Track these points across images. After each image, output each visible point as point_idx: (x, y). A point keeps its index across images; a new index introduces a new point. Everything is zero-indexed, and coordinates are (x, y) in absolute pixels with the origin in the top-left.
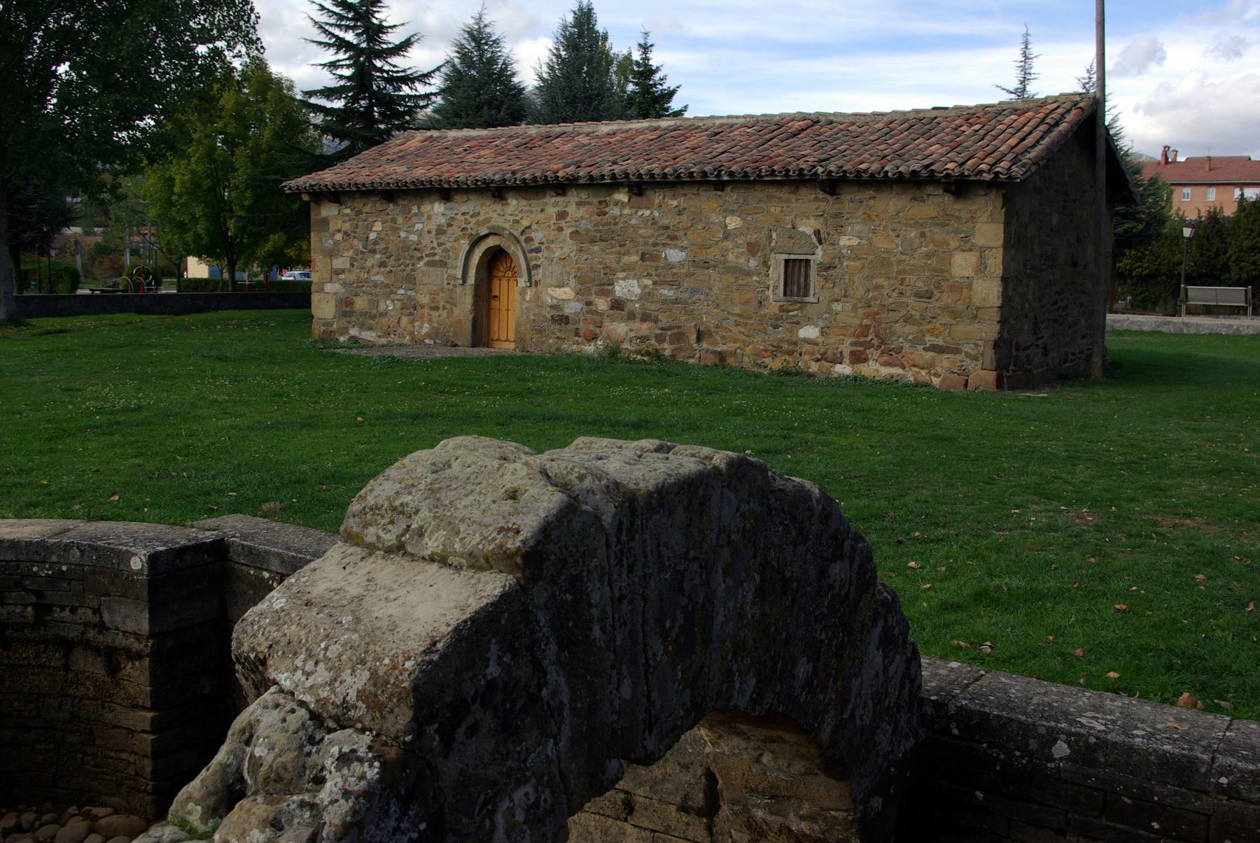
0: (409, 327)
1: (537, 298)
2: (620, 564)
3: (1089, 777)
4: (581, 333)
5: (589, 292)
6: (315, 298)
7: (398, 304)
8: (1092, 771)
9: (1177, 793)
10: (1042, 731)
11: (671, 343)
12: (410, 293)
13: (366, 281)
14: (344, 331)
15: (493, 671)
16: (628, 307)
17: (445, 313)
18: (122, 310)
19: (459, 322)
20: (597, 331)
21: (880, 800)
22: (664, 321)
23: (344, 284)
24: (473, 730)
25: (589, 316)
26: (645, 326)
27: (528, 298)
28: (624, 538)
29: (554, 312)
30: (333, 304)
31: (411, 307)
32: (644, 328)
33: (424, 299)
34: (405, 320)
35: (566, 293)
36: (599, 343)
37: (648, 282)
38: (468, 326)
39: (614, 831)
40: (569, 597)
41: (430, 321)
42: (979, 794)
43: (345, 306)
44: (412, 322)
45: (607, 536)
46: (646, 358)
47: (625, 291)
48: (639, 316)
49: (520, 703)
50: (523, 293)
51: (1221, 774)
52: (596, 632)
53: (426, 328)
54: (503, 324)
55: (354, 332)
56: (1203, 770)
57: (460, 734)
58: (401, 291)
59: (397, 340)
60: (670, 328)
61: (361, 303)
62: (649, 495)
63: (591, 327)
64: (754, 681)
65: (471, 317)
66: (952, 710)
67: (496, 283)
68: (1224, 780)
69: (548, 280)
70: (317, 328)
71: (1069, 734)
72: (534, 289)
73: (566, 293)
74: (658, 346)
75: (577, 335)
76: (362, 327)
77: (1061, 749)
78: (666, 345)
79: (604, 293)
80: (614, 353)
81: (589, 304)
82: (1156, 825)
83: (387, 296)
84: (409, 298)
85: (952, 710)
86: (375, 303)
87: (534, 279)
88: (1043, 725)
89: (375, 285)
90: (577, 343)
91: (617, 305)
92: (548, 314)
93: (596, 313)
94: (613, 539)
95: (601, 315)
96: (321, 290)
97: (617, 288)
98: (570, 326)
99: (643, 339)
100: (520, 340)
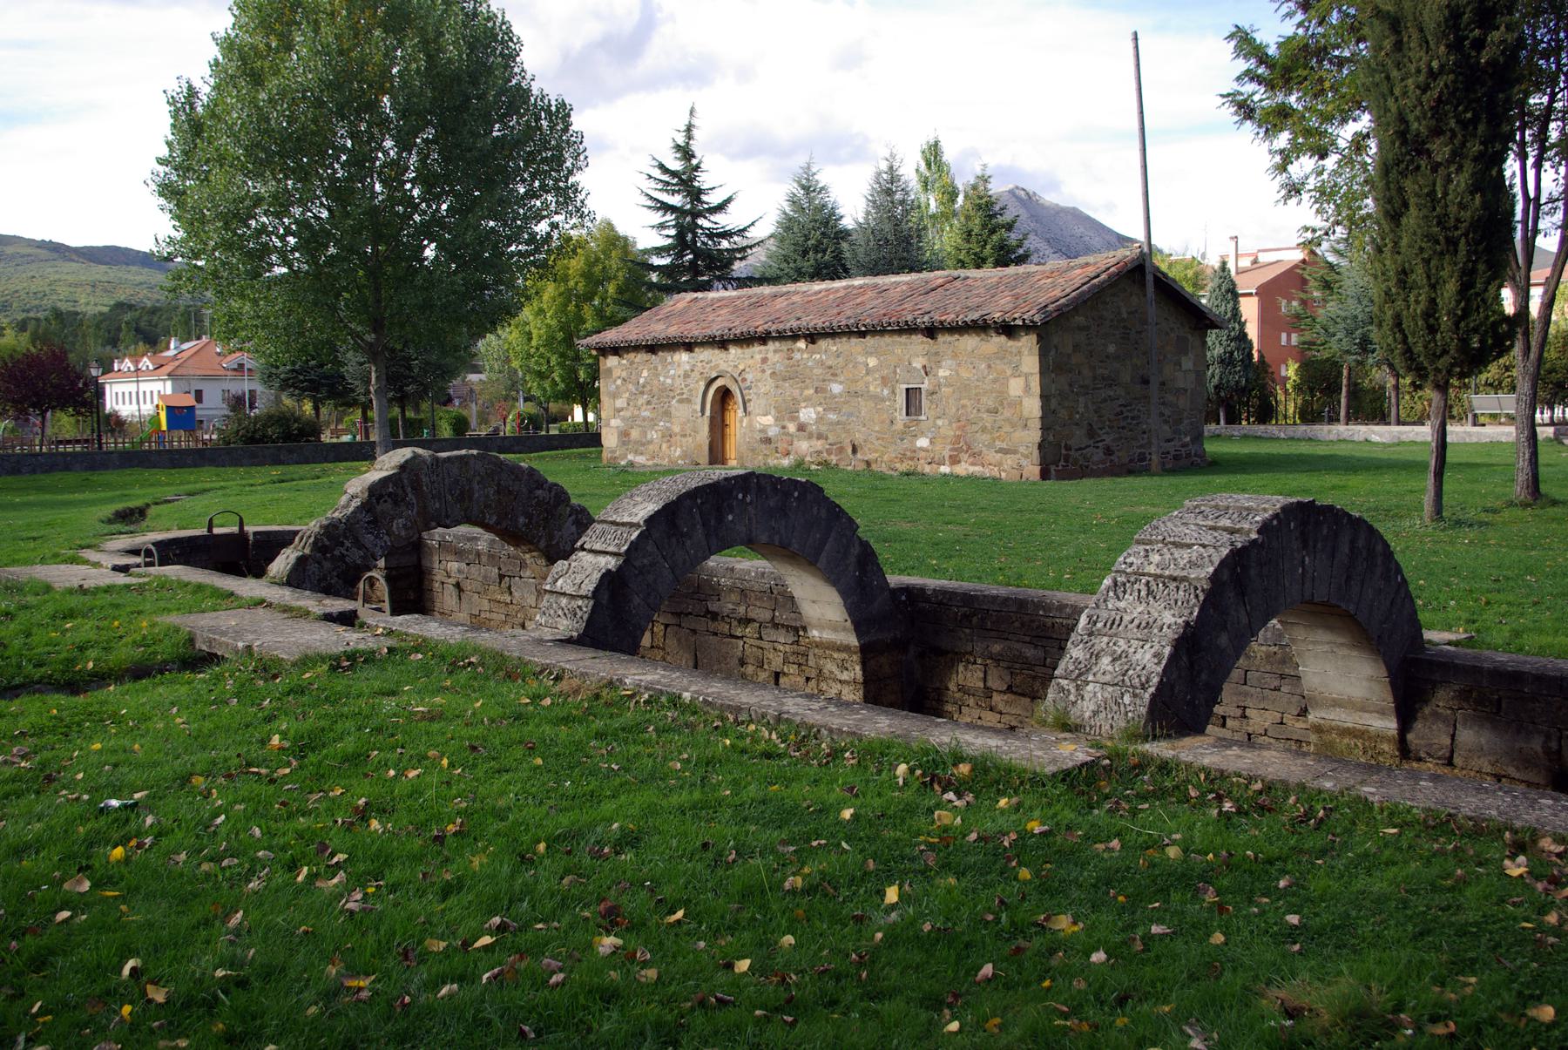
1: (750, 425)
6: (604, 432)
13: (638, 416)
16: (809, 429)
17: (690, 439)
19: (700, 446)
22: (832, 439)
23: (623, 419)
30: (616, 435)
31: (668, 436)
32: (819, 445)
33: (677, 429)
34: (664, 446)
35: (768, 420)
37: (820, 409)
41: (681, 446)
43: (624, 434)
44: (670, 447)
50: (741, 422)
55: (630, 457)
61: (635, 434)
70: (605, 455)
76: (636, 452)
86: (644, 433)
89: (644, 420)
91: (802, 428)
92: (758, 436)
93: (788, 434)
96: (608, 425)
98: (773, 445)
99: (819, 453)
100: (740, 458)
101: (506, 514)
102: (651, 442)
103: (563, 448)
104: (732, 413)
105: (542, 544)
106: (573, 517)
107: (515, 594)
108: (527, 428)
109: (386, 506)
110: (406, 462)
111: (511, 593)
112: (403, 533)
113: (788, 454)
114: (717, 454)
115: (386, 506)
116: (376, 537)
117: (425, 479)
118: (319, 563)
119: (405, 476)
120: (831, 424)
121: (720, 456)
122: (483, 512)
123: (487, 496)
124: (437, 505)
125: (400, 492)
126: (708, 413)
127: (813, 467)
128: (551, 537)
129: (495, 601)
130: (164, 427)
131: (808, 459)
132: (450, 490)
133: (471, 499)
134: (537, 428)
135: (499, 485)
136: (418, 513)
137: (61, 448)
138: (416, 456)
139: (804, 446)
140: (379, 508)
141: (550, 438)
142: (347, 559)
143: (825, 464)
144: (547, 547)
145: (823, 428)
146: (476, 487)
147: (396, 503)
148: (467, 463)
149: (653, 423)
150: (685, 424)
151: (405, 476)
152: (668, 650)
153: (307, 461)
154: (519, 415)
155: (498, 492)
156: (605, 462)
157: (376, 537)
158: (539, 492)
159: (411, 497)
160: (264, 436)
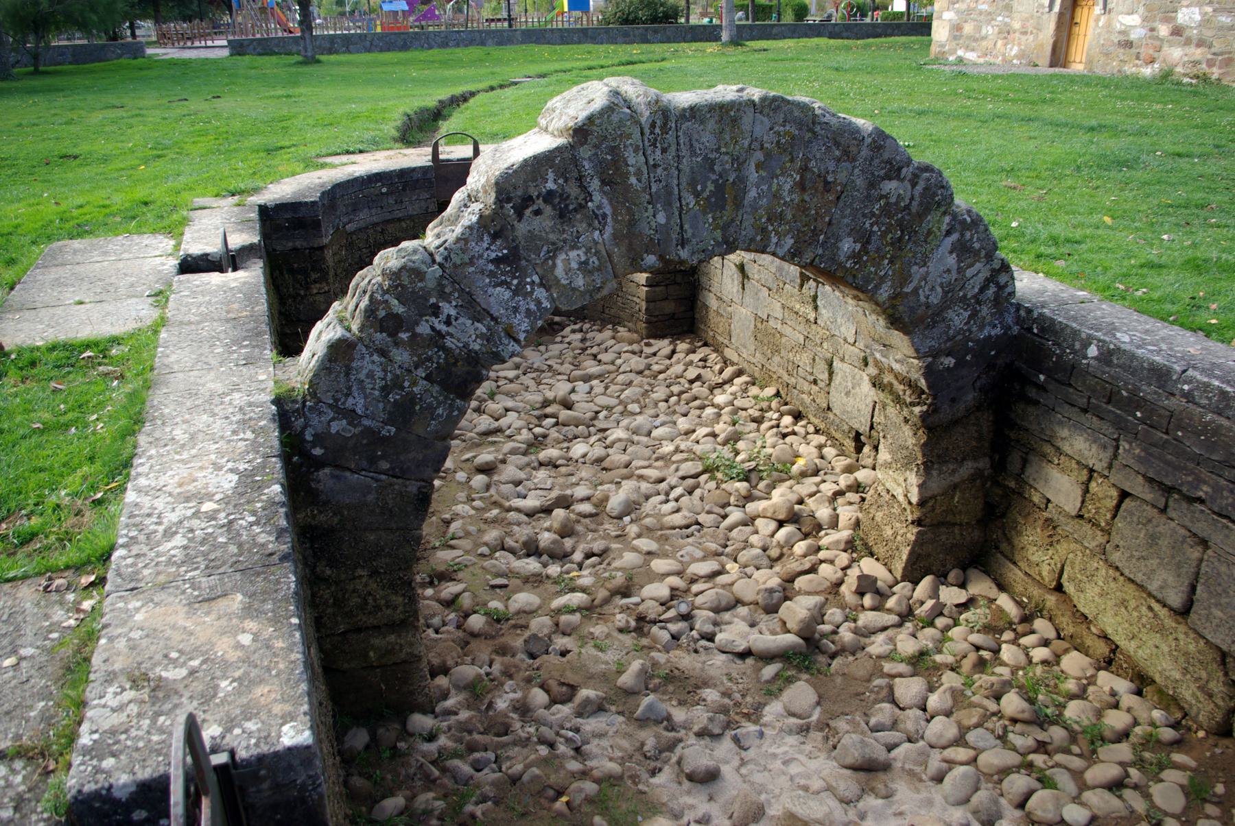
0: (1002, 50)
1: (1109, 24)
2: (654, 145)
3: (1104, 373)
4: (1142, 57)
5: (1153, 19)
6: (935, 24)
7: (996, 29)
8: (1107, 369)
9: (1156, 393)
10: (1084, 336)
11: (1220, 68)
12: (1007, 20)
13: (974, 9)
14: (953, 52)
15: (551, 185)
16: (1187, 33)
17: (1031, 38)
18: (819, 35)
19: (1042, 45)
20: (1156, 55)
21: (953, 361)
22: (1217, 47)
23: (958, 12)
24: (537, 213)
25: (1150, 41)
26: (1199, 51)
27: (1101, 24)
28: (657, 130)
29: (1122, 38)
30: (947, 29)
31: (1006, 32)
32: (1198, 53)
33: (1017, 25)
34: (1000, 43)
35: (1134, 20)
36: (1156, 66)
37: (1209, 9)
38: (1048, 49)
39: (857, 377)
40: (609, 157)
41: (1019, 44)
42: (1042, 377)
43: (957, 28)
44: (1005, 45)
45: (642, 129)
46: (1194, 81)
47: (1187, 18)
48: (1195, 42)
49: (571, 207)
50: (1097, 20)
51: (1185, 382)
52: (633, 180)
53: (1015, 51)
54: (1080, 48)
55: (960, 53)
56: (1174, 378)
57: (528, 212)
58: (1000, 18)
59: (992, 60)
60: (1221, 54)
61: (968, 28)
62: (684, 110)
63: (1151, 52)
64: (792, 241)
65: (1051, 41)
66: (1035, 315)
67: (1079, 10)
68: (1186, 387)
69: (1120, 8)
70: (934, 49)
71: (1099, 341)
72: (1107, 16)
73: (1134, 20)
74: (1208, 70)
75: (1138, 58)
76: (967, 48)
77: (1093, 351)
78: (1215, 70)
79: (1166, 20)
80: (1166, 75)
81: (1152, 30)
82: (1139, 414)
83: (989, 22)
84: (1006, 24)
85: (1035, 315)
86: (979, 29)
87: (1109, 7)
88: (1085, 331)
89: (981, 13)
90: (1137, 66)
91: (1177, 31)
92: (1116, 38)
93: (1157, 38)
94: (647, 131)
95: (1162, 40)
96: (940, 17)
97: (1180, 15)
98: (1134, 51)
99: (1196, 63)
100: (1090, 62)
101: (815, 233)
102: (984, 38)
103: (886, 36)
104: (1086, 10)
105: (884, 293)
106: (955, 237)
107: (823, 311)
108: (855, 15)
109: (540, 223)
110: (590, 119)
111: (816, 308)
112: (580, 282)
113: (1152, 61)
114: (1059, 55)
115: (540, 223)
116: (516, 293)
117: (634, 160)
118: (383, 353)
119: (585, 152)
120: (1221, 28)
121: (1062, 60)
122: (764, 230)
123: (776, 196)
124: (661, 218)
125: (573, 190)
126: (1057, 8)
127: (1186, 80)
128: (904, 278)
129: (791, 309)
130: (566, 9)
131: (1179, 69)
132: (692, 183)
133: (738, 204)
134: (864, 15)
135: (805, 169)
136: (615, 236)
137: (493, 25)
138: (617, 102)
139: (1176, 54)
140: (522, 228)
141: (874, 26)
142: (449, 342)
143: (1205, 79)
144: (893, 298)
145: (1208, 33)
146: (753, 175)
147: (563, 215)
148: (735, 121)
149: (990, 16)
150: (1027, 20)
151: (585, 152)
152: (1116, 539)
153: (668, 40)
154: (850, 4)
155: (802, 186)
156: (932, 56)
157: (516, 293)
158: (890, 186)
159: (599, 199)
160: (636, 18)
